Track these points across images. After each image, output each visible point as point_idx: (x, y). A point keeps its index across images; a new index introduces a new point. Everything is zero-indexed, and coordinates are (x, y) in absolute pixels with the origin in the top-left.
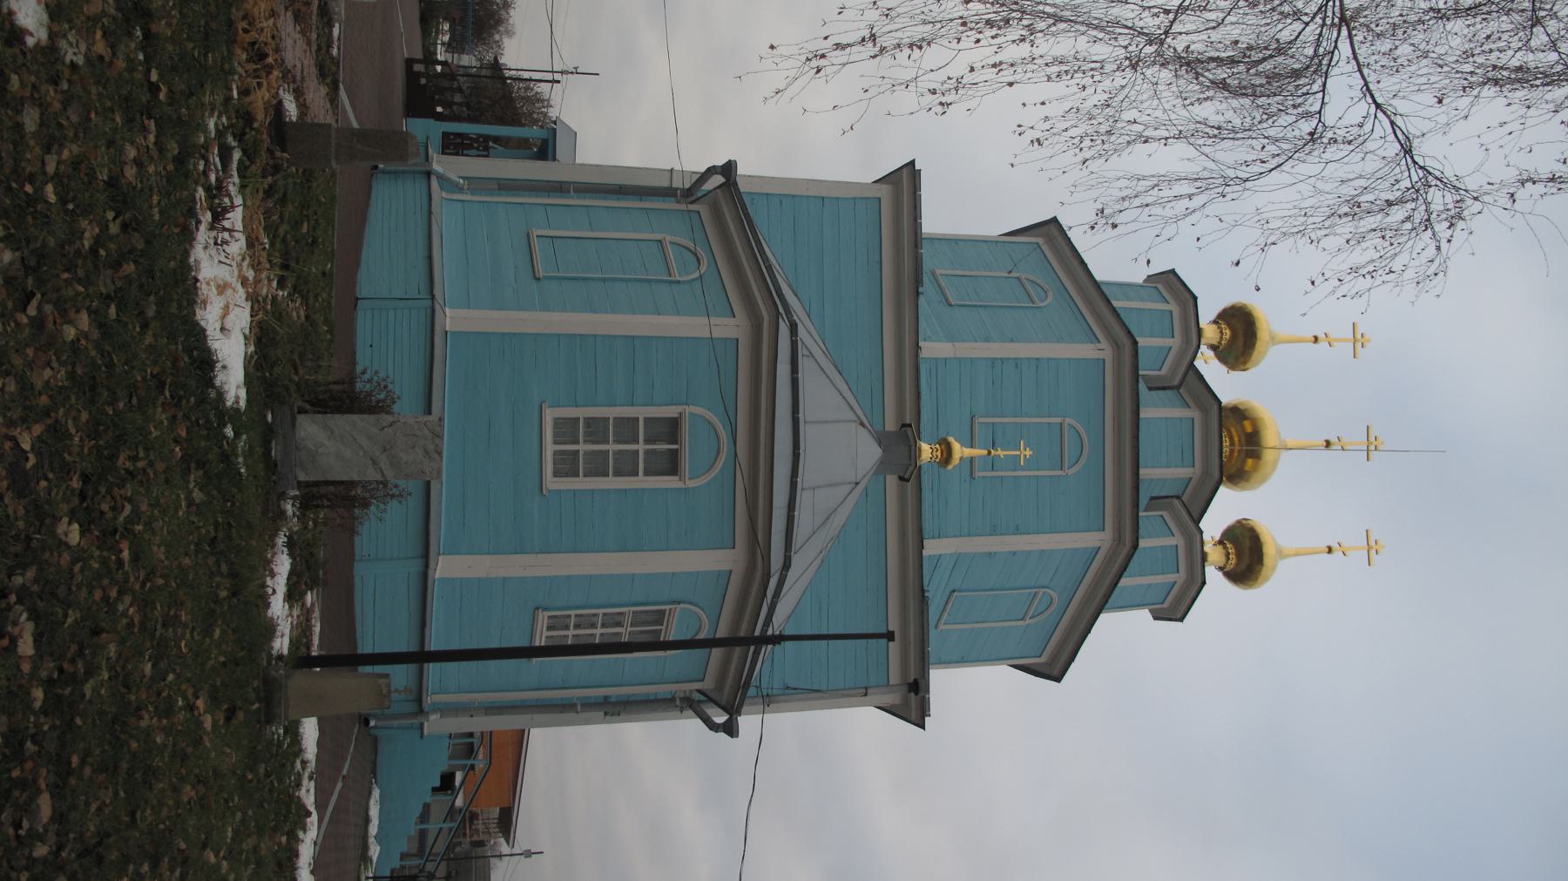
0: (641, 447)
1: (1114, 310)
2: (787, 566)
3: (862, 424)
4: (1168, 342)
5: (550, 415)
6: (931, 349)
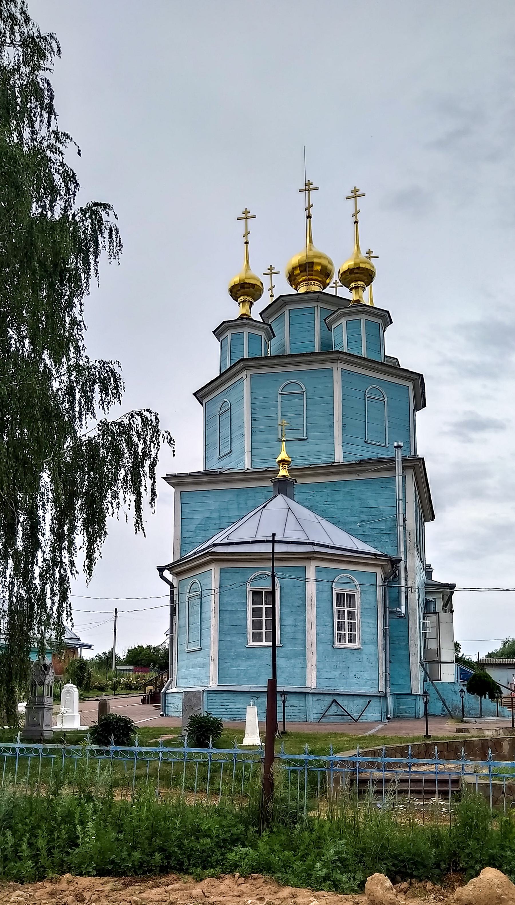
0: (264, 606)
1: (231, 368)
2: (312, 544)
3: (264, 507)
4: (246, 335)
5: (251, 644)
6: (247, 464)
